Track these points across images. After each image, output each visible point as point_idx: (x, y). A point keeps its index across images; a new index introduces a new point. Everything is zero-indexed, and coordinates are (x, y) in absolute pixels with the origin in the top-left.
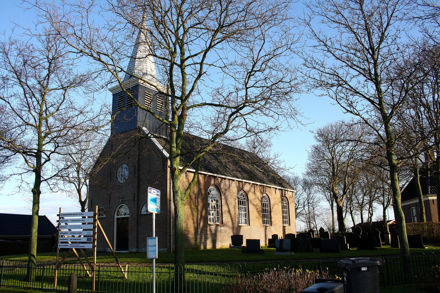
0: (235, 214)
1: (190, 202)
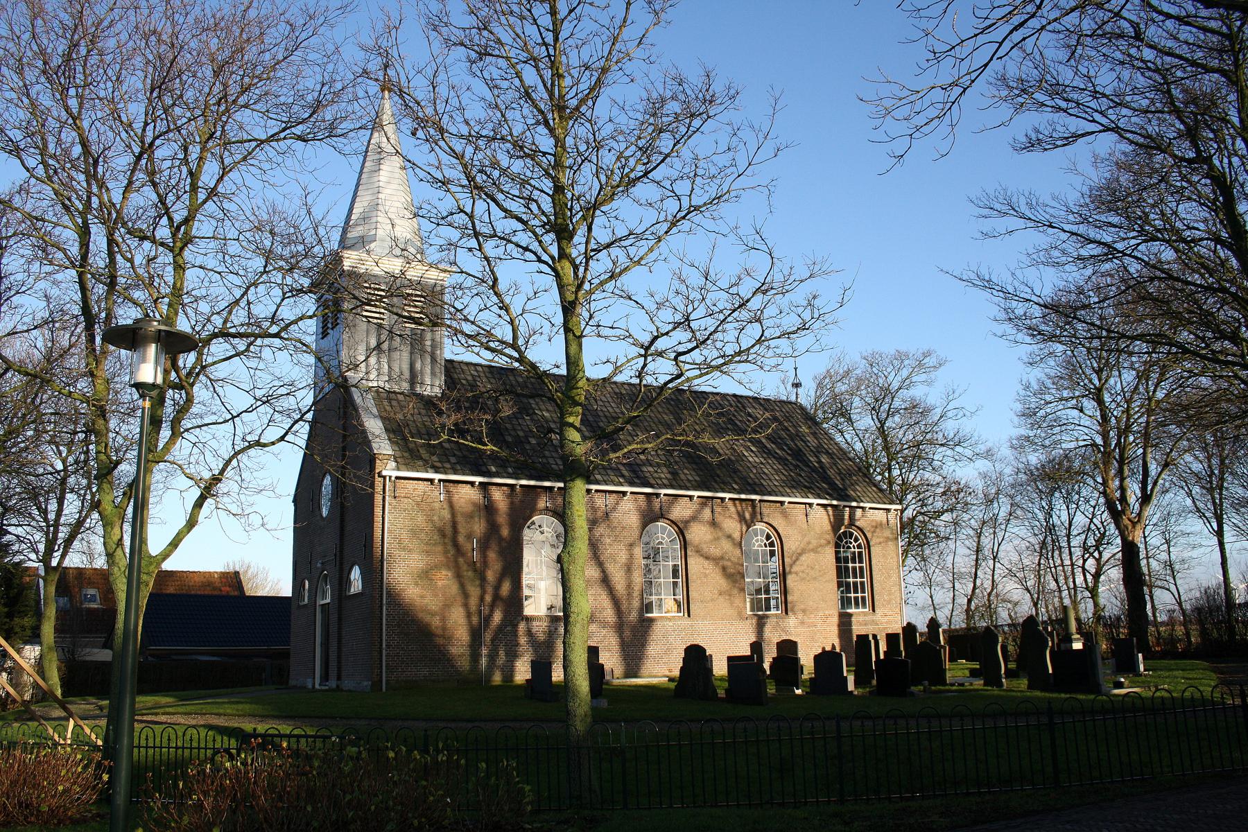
0: (629, 586)
1: (456, 562)
